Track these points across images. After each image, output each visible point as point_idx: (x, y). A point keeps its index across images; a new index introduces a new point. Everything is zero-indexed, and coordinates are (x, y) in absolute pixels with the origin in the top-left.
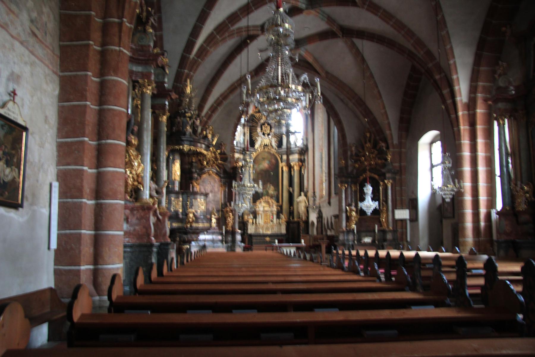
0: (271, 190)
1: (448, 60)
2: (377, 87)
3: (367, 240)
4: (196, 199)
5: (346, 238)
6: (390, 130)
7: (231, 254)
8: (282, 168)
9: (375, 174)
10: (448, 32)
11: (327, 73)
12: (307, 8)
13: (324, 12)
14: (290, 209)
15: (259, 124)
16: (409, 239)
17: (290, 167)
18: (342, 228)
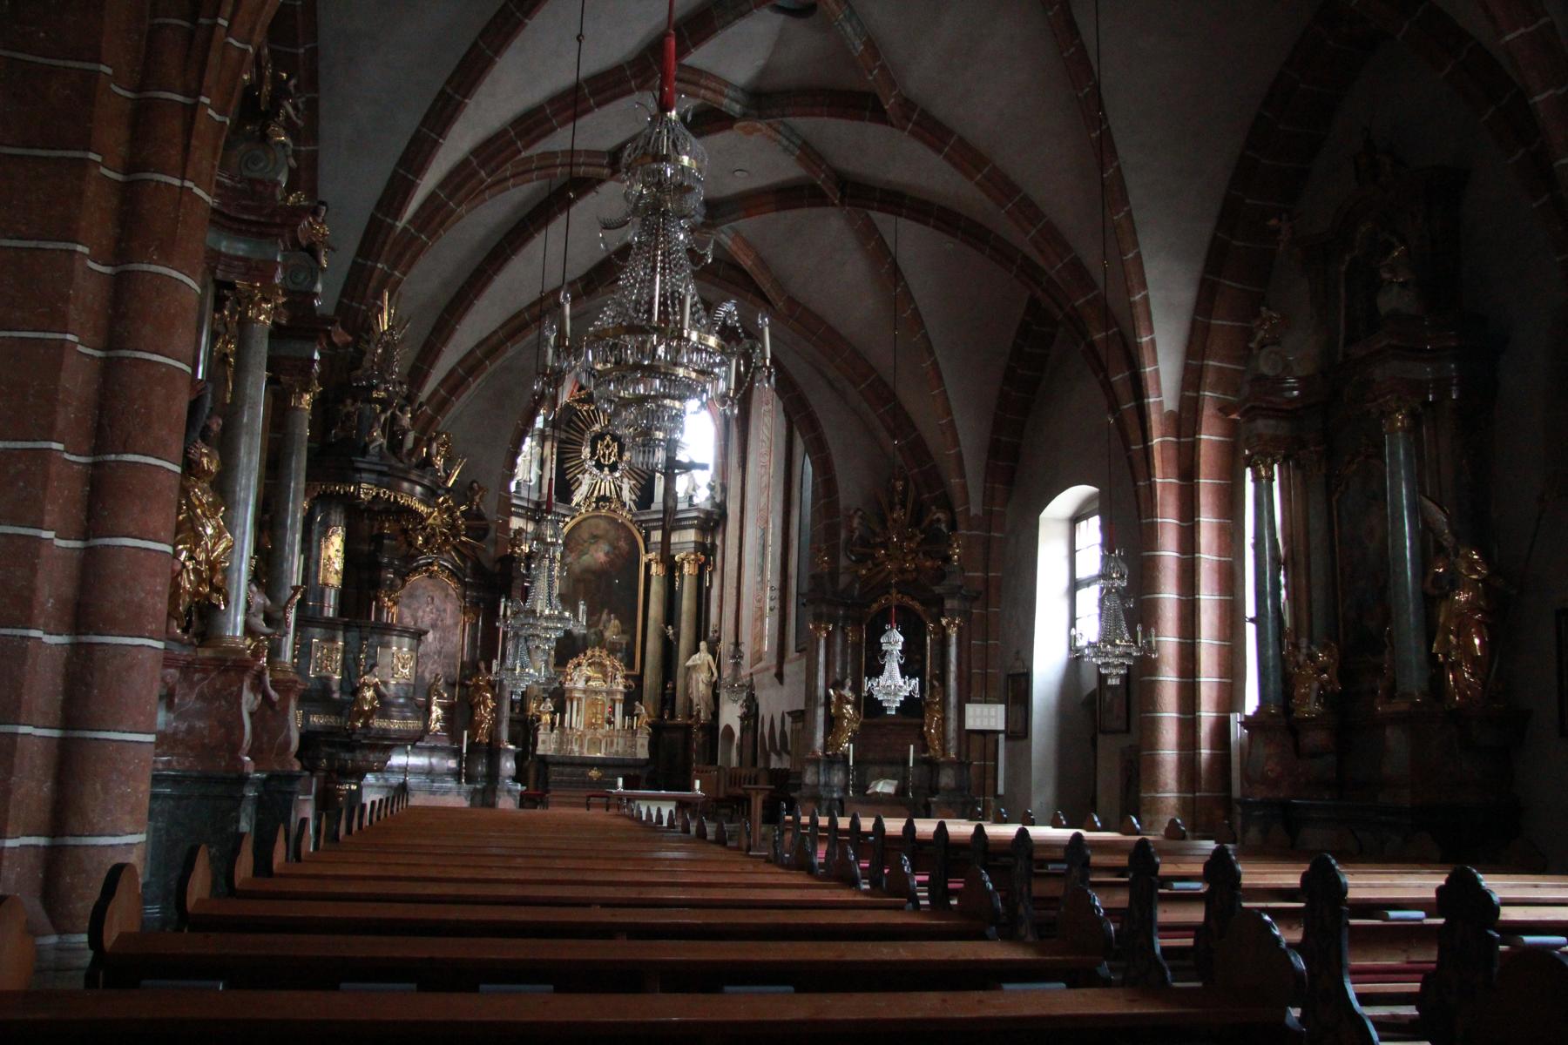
0: (612, 630)
1: (1129, 293)
2: (932, 353)
3: (885, 787)
4: (387, 646)
5: (822, 779)
6: (962, 476)
7: (486, 812)
8: (648, 567)
9: (913, 599)
10: (1129, 215)
11: (792, 302)
12: (745, 116)
13: (792, 130)
14: (664, 688)
15: (588, 436)
16: (1001, 790)
17: (671, 567)
18: (814, 752)
